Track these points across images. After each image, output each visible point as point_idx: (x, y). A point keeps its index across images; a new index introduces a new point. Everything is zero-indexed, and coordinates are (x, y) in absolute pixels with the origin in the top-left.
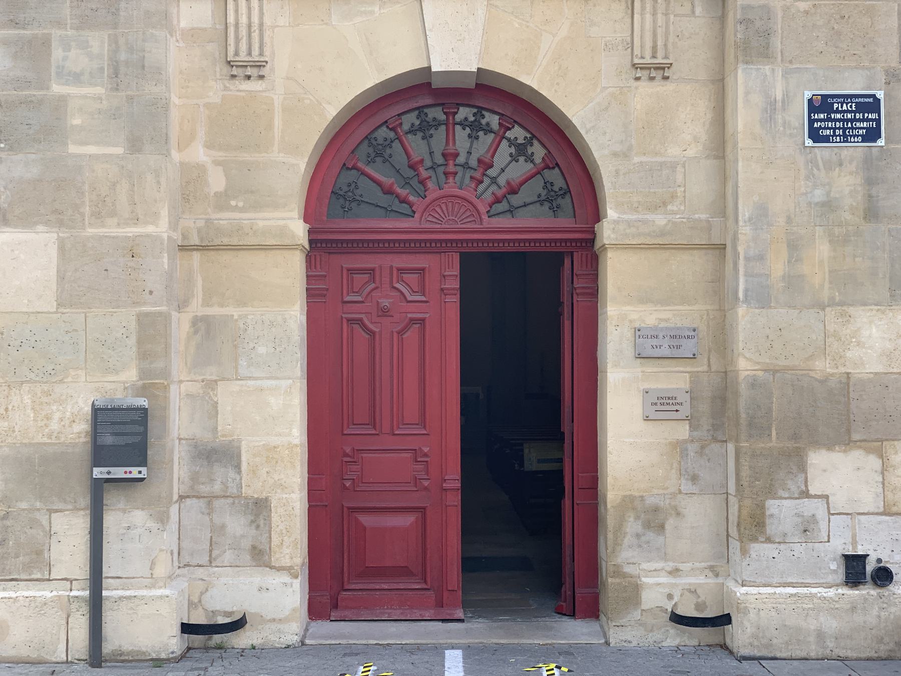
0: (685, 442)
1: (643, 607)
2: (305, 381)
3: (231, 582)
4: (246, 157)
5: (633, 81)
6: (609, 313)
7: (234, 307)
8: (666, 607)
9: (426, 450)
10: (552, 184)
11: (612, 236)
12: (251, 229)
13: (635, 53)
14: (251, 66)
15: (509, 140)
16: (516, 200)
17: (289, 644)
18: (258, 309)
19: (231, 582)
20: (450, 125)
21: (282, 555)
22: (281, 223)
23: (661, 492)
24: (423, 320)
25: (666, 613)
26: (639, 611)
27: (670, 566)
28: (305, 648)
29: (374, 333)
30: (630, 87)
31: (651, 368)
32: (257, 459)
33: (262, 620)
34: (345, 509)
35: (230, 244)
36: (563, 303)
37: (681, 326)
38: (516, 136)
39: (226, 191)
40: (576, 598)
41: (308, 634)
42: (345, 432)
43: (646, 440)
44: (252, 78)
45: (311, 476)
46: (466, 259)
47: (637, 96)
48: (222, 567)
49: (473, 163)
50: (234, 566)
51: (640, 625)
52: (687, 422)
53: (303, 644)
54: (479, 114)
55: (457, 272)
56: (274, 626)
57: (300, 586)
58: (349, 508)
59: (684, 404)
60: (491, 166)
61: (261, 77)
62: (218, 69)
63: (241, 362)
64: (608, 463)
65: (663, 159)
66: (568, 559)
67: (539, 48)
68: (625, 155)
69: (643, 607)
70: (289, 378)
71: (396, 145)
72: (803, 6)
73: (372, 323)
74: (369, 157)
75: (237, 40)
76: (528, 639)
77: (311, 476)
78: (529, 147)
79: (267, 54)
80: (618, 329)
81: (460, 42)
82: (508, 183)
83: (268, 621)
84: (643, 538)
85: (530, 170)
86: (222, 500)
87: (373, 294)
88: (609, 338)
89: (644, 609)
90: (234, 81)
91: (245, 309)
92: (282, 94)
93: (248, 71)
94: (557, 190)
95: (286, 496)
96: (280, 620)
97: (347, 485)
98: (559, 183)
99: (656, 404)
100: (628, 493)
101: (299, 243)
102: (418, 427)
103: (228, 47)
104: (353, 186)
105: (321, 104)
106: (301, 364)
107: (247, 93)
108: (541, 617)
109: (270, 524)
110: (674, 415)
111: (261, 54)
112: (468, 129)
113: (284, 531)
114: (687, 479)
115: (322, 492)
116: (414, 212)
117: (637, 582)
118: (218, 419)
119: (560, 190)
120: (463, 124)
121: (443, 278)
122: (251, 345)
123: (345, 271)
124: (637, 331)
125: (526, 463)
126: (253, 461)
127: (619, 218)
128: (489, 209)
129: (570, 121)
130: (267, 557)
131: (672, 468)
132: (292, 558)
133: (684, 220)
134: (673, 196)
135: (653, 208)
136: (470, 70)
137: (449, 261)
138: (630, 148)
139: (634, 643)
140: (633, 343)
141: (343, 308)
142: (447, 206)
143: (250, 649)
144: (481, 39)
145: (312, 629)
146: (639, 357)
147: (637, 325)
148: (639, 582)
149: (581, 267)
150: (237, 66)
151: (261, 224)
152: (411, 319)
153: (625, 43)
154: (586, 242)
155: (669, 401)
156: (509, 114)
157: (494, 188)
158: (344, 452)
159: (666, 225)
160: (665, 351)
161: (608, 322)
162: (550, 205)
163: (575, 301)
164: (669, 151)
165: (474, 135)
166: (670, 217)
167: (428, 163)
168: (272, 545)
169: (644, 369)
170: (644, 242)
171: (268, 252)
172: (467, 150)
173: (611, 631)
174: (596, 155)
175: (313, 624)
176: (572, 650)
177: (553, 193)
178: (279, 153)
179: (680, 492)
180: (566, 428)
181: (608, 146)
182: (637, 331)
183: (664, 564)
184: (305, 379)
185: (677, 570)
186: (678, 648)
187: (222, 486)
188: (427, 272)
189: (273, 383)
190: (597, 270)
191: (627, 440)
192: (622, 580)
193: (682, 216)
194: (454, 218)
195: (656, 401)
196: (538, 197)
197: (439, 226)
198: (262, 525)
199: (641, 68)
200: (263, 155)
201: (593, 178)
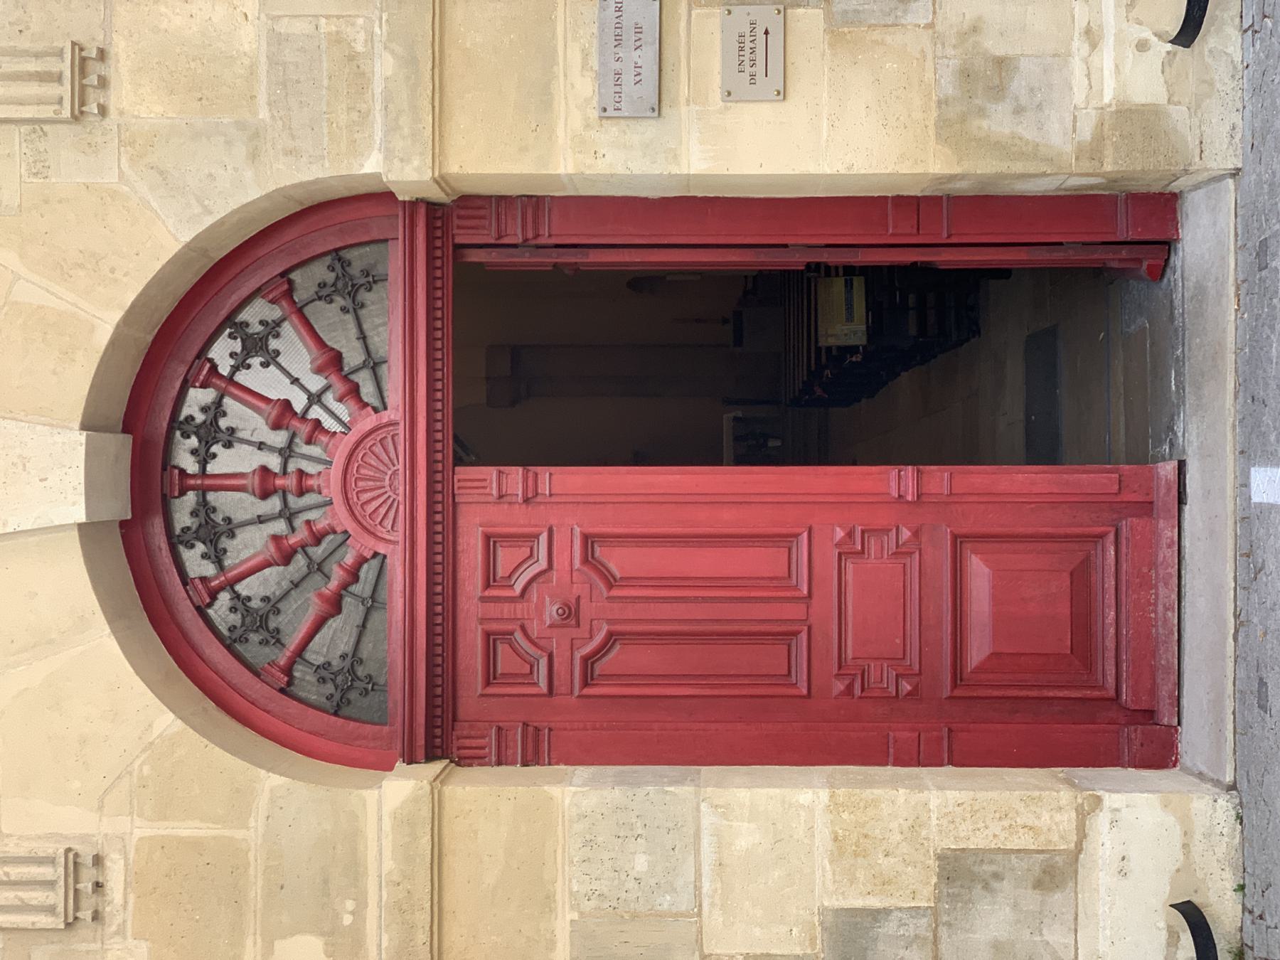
0: (829, 17)
1: (1162, 99)
2: (705, 770)
3: (1108, 932)
4: (256, 891)
5: (107, 120)
6: (571, 170)
7: (556, 919)
8: (1164, 54)
9: (840, 533)
10: (322, 285)
11: (416, 163)
12: (398, 884)
13: (51, 115)
14: (76, 881)
15: (235, 369)
16: (353, 357)
17: (1234, 817)
18: (560, 871)
19: (1108, 932)
20: (206, 484)
21: (1054, 827)
22: (387, 824)
23: (929, 64)
24: (586, 538)
25: (1175, 54)
26: (1171, 107)
27: (1079, 46)
28: (1243, 785)
29: (610, 634)
30: (118, 126)
31: (680, 87)
32: (861, 875)
33: (1184, 870)
34: (957, 693)
35: (428, 928)
36: (555, 265)
37: (596, 25)
38: (227, 354)
39: (322, 934)
40: (1137, 238)
41: (1211, 775)
42: (805, 691)
43: (825, 95)
44: (101, 880)
45: (891, 759)
46: (466, 453)
47: (136, 113)
48: (1077, 949)
49: (280, 438)
50: (1076, 924)
51: (1198, 106)
52: (789, 11)
53: (1233, 787)
54: (187, 426)
55: (492, 472)
56: (1198, 847)
57: (1118, 792)
58: (955, 685)
59: (752, 18)
60: (287, 404)
61: (98, 861)
62: (83, 947)
63: (666, 906)
64: (871, 172)
65: (263, 59)
66: (1057, 255)
67: (40, 307)
68: (255, 137)
69: (1162, 99)
70: (698, 809)
71: (242, 588)
72: (1277, 821)
73: (591, 638)
74: (268, 642)
75: (24, 908)
76: (1224, 331)
77: (891, 759)
78: (250, 331)
79: (50, 851)
80: (603, 151)
81: (27, 465)
82: (318, 371)
83: (1188, 858)
84: (1024, 100)
85: (294, 327)
86: (943, 947)
87: (534, 635)
88: (620, 170)
89: (1166, 98)
90: (106, 915)
91: (558, 897)
92: (132, 820)
93: (86, 887)
94: (333, 275)
95: (934, 816)
96: (1186, 833)
97: (909, 688)
98: (320, 272)
99: (753, 76)
100: (932, 132)
101: (428, 788)
102: (794, 550)
103: (38, 926)
104: (324, 673)
105: (151, 743)
106: (670, 784)
107: (129, 890)
108: (1172, 308)
109: (990, 851)
110: (775, 40)
111: (51, 861)
112: (215, 449)
113: (1006, 823)
114: (905, 12)
115: (922, 738)
116: (376, 555)
117: (1112, 112)
118: (779, 953)
119: (333, 270)
120: (205, 457)
121: (505, 499)
122: (631, 884)
123: (490, 690)
124: (606, 114)
125: (853, 341)
126: (864, 884)
127: (380, 150)
128: (369, 409)
129: (188, 246)
130: (1057, 858)
131: (883, 43)
132: (1061, 808)
133: (384, 18)
134: (337, 39)
135: (361, 81)
136: (84, 446)
137: (470, 488)
138: (241, 125)
139: (1236, 118)
140: (631, 122)
141: (561, 694)
142: (365, 491)
143: (1244, 895)
144: (23, 424)
145: (1199, 764)
146: (658, 109)
147: (594, 114)
148: (1113, 108)
149: (484, 228)
150: (77, 908)
151: (388, 865)
152: (585, 561)
153: (33, 136)
154: (435, 218)
155: (748, 51)
156: (182, 370)
157: (329, 399)
158: (842, 694)
159: (393, 52)
160: (647, 57)
161: (588, 172)
162: (362, 290)
163: (554, 241)
164: (246, 47)
165: (226, 437)
166: (378, 47)
167: (280, 527)
168: (1033, 847)
169: (682, 100)
170: (429, 99)
171: (445, 851)
172: (256, 449)
173: (1213, 165)
174: (253, 194)
175: (1186, 759)
176: (1254, 242)
177: (340, 285)
178: (248, 828)
179: (931, 26)
180: (797, 260)
181: (236, 169)
182: (606, 114)
183: (1077, 58)
184: (699, 772)
185: (1088, 31)
186: (1246, 31)
187: (915, 946)
188: (490, 530)
189: (706, 841)
190: (488, 198)
191: (825, 134)
192: (1108, 142)
193: (377, 22)
194: (387, 478)
195: (746, 76)
196: (348, 312)
197: (401, 507)
198: (993, 868)
199: (82, 104)
200: (251, 858)
201: (307, 204)
